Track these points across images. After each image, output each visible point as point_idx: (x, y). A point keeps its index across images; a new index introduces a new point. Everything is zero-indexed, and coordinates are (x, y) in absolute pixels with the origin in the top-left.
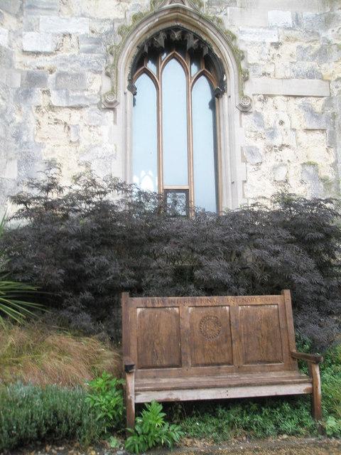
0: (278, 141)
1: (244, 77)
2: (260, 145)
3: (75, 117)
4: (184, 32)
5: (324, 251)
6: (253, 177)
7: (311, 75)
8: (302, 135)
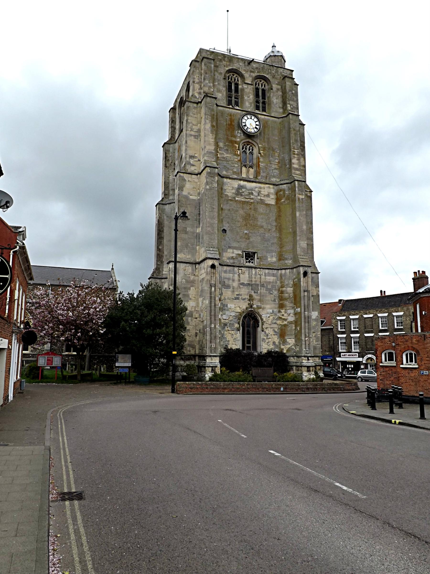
0: (269, 337)
1: (263, 324)
2: (265, 338)
3: (233, 332)
4: (252, 314)
5: (153, 330)
6: (264, 344)
7: (275, 323)
8: (273, 336)
